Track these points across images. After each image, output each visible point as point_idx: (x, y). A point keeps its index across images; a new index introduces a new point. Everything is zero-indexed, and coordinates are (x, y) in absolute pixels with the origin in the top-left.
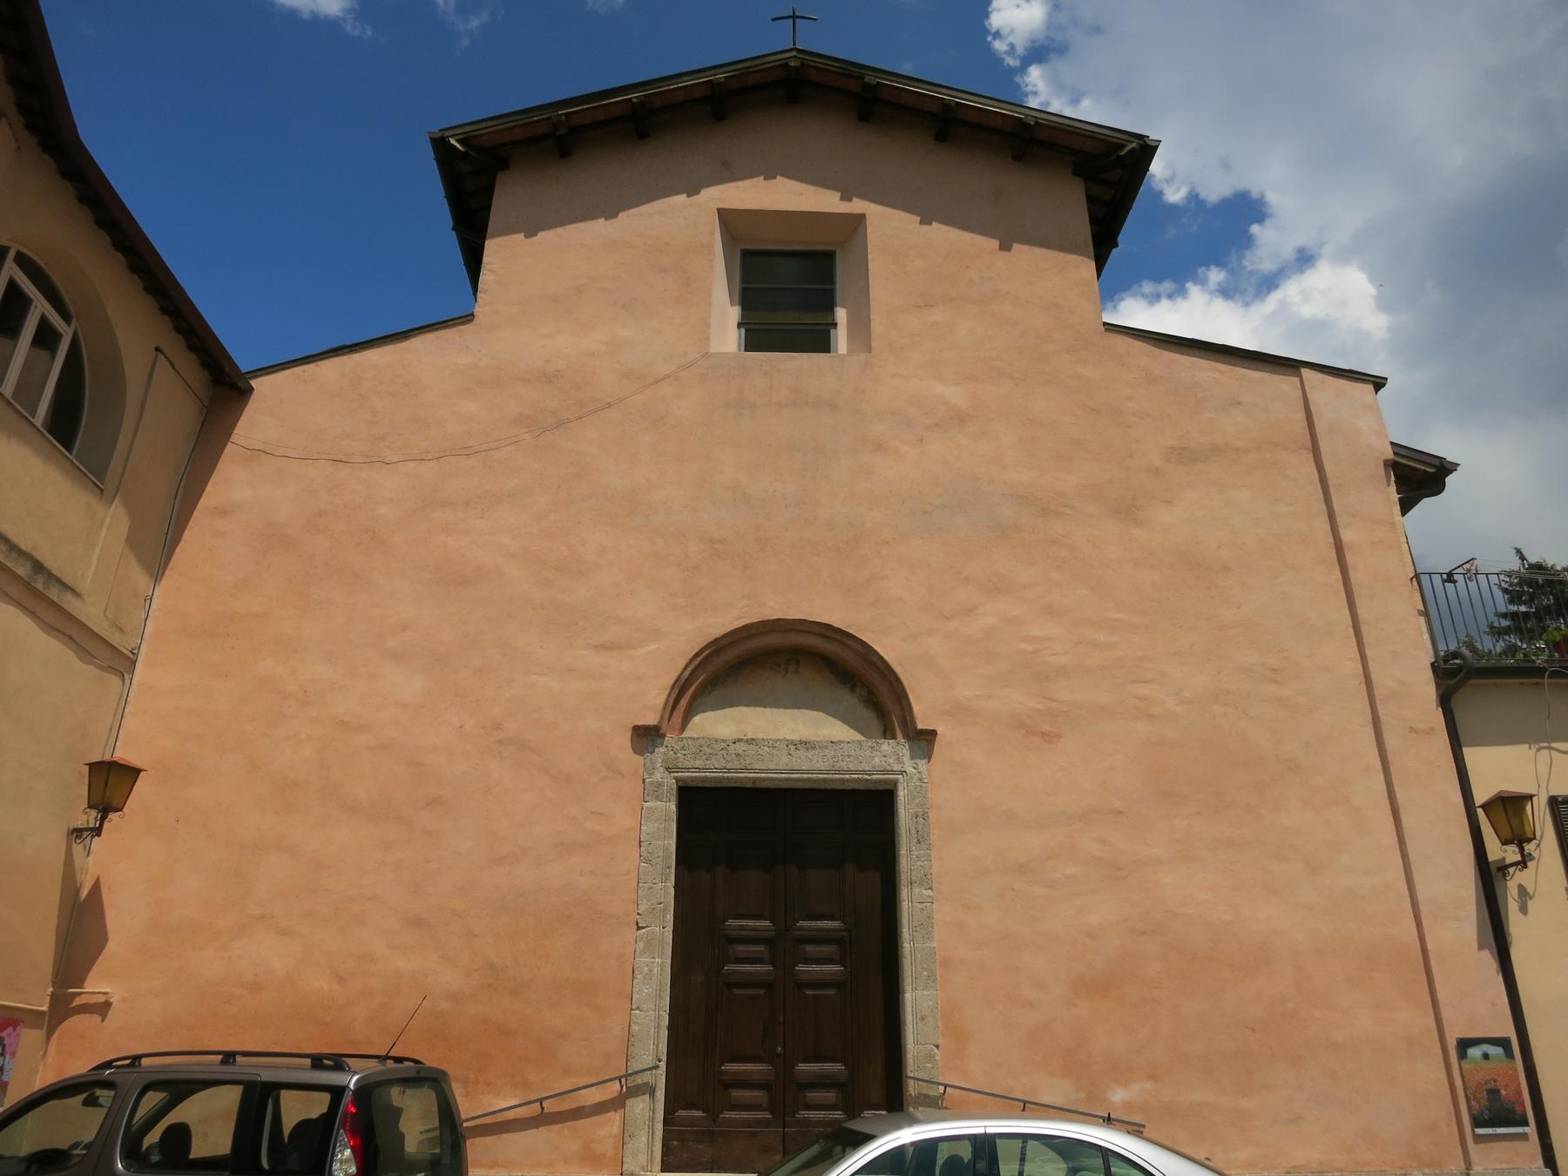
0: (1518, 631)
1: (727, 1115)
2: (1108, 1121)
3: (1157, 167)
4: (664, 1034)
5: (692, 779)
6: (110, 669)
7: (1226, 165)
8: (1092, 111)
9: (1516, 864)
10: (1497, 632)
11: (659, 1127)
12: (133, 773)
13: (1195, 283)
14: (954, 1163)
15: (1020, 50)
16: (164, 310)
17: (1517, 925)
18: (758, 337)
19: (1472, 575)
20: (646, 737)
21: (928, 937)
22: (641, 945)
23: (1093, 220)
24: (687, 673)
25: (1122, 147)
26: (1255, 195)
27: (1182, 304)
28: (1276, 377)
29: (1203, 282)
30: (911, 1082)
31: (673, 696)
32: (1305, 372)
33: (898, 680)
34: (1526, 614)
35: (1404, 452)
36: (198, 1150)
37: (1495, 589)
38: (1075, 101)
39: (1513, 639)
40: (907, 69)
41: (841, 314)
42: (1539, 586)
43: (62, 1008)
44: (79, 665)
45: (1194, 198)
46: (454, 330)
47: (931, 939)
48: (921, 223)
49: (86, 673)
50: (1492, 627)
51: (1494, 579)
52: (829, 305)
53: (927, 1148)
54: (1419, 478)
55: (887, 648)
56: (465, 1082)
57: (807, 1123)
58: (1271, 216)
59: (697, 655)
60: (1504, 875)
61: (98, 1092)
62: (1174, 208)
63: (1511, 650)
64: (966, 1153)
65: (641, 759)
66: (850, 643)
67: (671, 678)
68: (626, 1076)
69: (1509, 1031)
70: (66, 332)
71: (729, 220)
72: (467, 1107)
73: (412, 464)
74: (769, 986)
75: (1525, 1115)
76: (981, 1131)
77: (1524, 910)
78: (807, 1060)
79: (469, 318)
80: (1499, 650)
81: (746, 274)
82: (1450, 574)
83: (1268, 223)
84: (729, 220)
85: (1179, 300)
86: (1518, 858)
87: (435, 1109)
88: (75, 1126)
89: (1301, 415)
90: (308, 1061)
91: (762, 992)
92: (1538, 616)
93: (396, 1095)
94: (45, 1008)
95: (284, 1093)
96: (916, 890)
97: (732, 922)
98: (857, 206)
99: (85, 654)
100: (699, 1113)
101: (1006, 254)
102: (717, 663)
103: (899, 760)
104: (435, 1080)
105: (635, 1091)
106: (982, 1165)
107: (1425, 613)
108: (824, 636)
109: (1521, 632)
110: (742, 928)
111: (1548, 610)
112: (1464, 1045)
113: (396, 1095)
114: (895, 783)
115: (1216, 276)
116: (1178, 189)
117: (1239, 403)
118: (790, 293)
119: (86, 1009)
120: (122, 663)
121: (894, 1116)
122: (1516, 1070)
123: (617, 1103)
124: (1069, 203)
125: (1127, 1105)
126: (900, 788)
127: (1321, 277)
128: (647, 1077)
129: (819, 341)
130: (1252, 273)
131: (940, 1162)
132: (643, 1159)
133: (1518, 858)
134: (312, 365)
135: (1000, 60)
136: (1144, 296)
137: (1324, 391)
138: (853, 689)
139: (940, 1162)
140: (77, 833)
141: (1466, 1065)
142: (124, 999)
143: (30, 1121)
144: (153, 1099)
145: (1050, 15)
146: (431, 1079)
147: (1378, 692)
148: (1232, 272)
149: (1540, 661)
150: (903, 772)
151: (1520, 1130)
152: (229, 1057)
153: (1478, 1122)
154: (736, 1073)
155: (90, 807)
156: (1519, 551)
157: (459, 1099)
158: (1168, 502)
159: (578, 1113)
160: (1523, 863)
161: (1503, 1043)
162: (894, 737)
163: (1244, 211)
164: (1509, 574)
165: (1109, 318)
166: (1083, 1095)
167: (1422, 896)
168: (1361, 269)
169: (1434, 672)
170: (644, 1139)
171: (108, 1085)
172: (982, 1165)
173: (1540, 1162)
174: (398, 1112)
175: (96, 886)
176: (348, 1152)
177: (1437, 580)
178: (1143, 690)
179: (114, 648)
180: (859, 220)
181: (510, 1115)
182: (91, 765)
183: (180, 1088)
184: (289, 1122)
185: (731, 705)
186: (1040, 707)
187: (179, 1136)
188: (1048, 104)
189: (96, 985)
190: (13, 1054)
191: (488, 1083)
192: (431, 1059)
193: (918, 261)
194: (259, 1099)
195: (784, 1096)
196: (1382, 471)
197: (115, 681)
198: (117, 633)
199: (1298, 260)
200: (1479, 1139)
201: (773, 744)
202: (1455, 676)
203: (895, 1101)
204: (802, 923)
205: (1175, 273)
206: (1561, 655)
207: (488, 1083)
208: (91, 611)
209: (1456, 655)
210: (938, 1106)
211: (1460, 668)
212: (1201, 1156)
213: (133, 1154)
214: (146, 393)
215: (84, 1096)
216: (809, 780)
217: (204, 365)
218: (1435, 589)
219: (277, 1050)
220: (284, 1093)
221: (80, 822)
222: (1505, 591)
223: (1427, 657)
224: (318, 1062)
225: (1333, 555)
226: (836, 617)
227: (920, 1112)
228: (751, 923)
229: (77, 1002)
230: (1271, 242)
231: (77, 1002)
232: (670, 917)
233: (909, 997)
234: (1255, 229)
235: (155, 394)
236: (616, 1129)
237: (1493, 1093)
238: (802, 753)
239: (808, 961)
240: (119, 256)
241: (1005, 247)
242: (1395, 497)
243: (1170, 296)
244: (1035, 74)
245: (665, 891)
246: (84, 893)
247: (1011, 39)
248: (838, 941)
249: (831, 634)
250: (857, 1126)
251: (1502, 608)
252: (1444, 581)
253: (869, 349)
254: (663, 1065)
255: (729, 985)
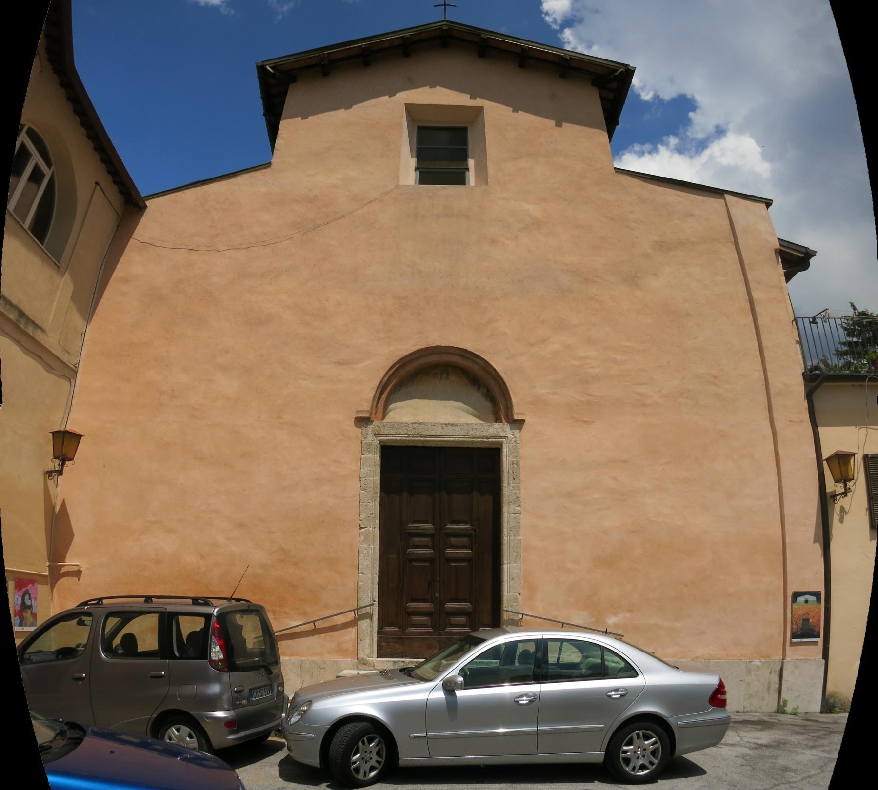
0: (851, 352)
1: (449, 629)
2: (606, 633)
3: (635, 81)
4: (376, 587)
5: (389, 441)
6: (62, 376)
7: (671, 80)
8: (598, 52)
9: (841, 494)
10: (840, 354)
11: (375, 635)
12: (78, 437)
13: (662, 145)
14: (525, 653)
15: (559, 21)
16: (103, 161)
17: (837, 529)
18: (426, 176)
19: (826, 319)
20: (362, 421)
21: (517, 534)
22: (362, 538)
23: (604, 110)
24: (386, 379)
25: (616, 70)
26: (689, 96)
27: (657, 157)
28: (711, 199)
29: (667, 144)
30: (505, 613)
31: (378, 393)
32: (727, 196)
33: (504, 383)
34: (856, 343)
35: (786, 244)
36: (141, 648)
37: (839, 327)
38: (589, 47)
39: (849, 358)
40: (502, 30)
41: (471, 163)
42: (864, 326)
43: (56, 575)
44: (45, 374)
45: (656, 97)
46: (260, 172)
47: (519, 535)
48: (513, 111)
49: (50, 379)
50: (837, 351)
51: (839, 321)
52: (464, 157)
53: (512, 646)
54: (795, 260)
55: (498, 364)
56: (274, 612)
57: (451, 634)
58: (699, 107)
59: (391, 368)
60: (834, 501)
61: (84, 618)
62: (647, 104)
63: (848, 365)
64: (532, 648)
65: (360, 430)
66: (478, 360)
67: (377, 382)
68: (358, 609)
69: (821, 588)
70: (47, 172)
71: (411, 110)
72: (277, 625)
73: (233, 251)
74: (431, 561)
75: (819, 632)
76: (540, 637)
77: (841, 520)
78: (451, 601)
79: (268, 165)
80: (841, 365)
81: (420, 141)
82: (814, 319)
83: (698, 111)
84: (411, 110)
85: (655, 155)
86: (843, 490)
87: (260, 626)
88: (75, 635)
89: (727, 222)
90: (190, 601)
91: (427, 564)
92: (863, 344)
93: (238, 619)
94: (47, 574)
95: (180, 617)
96: (512, 507)
97: (411, 525)
98: (479, 102)
99: (49, 368)
100: (396, 629)
101: (559, 129)
102: (403, 372)
103: (504, 430)
104: (258, 611)
105: (362, 617)
106: (540, 655)
107: (800, 342)
108: (462, 356)
109: (854, 354)
110: (417, 528)
111: (869, 340)
112: (796, 595)
113: (238, 619)
114: (501, 444)
115: (673, 141)
116: (648, 93)
117: (692, 215)
118: (443, 152)
119: (68, 574)
120: (69, 373)
121: (495, 629)
122: (820, 609)
123: (353, 623)
124: (591, 101)
125: (616, 625)
126: (504, 447)
127: (730, 141)
128: (368, 610)
129: (459, 179)
130: (693, 139)
131: (518, 653)
132: (367, 651)
133: (843, 490)
134: (180, 193)
135: (549, 26)
136: (635, 152)
137: (739, 208)
138: (479, 389)
139: (518, 653)
140: (49, 473)
141: (795, 606)
142: (88, 569)
143: (52, 632)
144: (113, 622)
145: (572, 4)
146: (257, 611)
147: (772, 391)
148: (682, 139)
149: (864, 371)
150: (506, 437)
151: (814, 640)
152: (148, 599)
153: (794, 636)
154: (415, 607)
155: (55, 458)
156: (852, 305)
157: (271, 621)
158: (655, 274)
159: (333, 628)
160: (845, 494)
161: (817, 594)
162: (501, 422)
163: (683, 107)
164: (847, 318)
165: (617, 165)
166: (593, 620)
167: (787, 512)
168: (751, 136)
169: (804, 378)
170: (368, 641)
171: (88, 614)
172: (540, 655)
173: (821, 656)
174: (240, 628)
175: (64, 504)
176: (218, 648)
177: (807, 321)
178: (641, 389)
179: (64, 364)
180: (481, 109)
181: (299, 629)
182: (54, 433)
183: (127, 616)
184: (185, 633)
185: (411, 398)
186: (583, 399)
187: (130, 641)
188: (576, 48)
189: (72, 561)
190: (35, 598)
191: (286, 613)
192: (255, 600)
193: (511, 131)
194: (168, 622)
195: (439, 619)
196: (774, 256)
197: (66, 383)
198: (66, 354)
199: (716, 132)
200: (793, 644)
201: (434, 424)
202: (816, 380)
203: (496, 623)
204: (449, 526)
205: (651, 139)
206: (876, 368)
207: (286, 613)
208: (51, 341)
209: (816, 368)
210: (517, 625)
211: (819, 376)
212: (650, 651)
213: (108, 649)
214: (88, 208)
215: (76, 620)
216: (454, 442)
217: (121, 192)
218: (805, 326)
219: (173, 595)
220: (180, 617)
221: (50, 467)
222: (845, 329)
223: (800, 369)
224: (195, 601)
225: (748, 306)
226: (469, 345)
227: (508, 628)
228: (422, 525)
229: (63, 570)
230: (701, 122)
231: (63, 570)
232: (378, 522)
233: (506, 567)
234: (691, 114)
235: (92, 205)
236: (353, 636)
237: (806, 621)
238: (450, 427)
239: (452, 547)
240: (83, 130)
241: (559, 125)
242: (782, 271)
243: (650, 153)
244: (568, 33)
245: (375, 507)
246: (57, 509)
247: (554, 16)
248: (468, 536)
249: (466, 355)
250: (477, 634)
251: (843, 340)
252: (811, 323)
253: (487, 183)
254: (376, 603)
255: (411, 560)
